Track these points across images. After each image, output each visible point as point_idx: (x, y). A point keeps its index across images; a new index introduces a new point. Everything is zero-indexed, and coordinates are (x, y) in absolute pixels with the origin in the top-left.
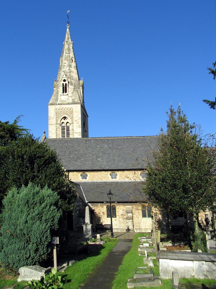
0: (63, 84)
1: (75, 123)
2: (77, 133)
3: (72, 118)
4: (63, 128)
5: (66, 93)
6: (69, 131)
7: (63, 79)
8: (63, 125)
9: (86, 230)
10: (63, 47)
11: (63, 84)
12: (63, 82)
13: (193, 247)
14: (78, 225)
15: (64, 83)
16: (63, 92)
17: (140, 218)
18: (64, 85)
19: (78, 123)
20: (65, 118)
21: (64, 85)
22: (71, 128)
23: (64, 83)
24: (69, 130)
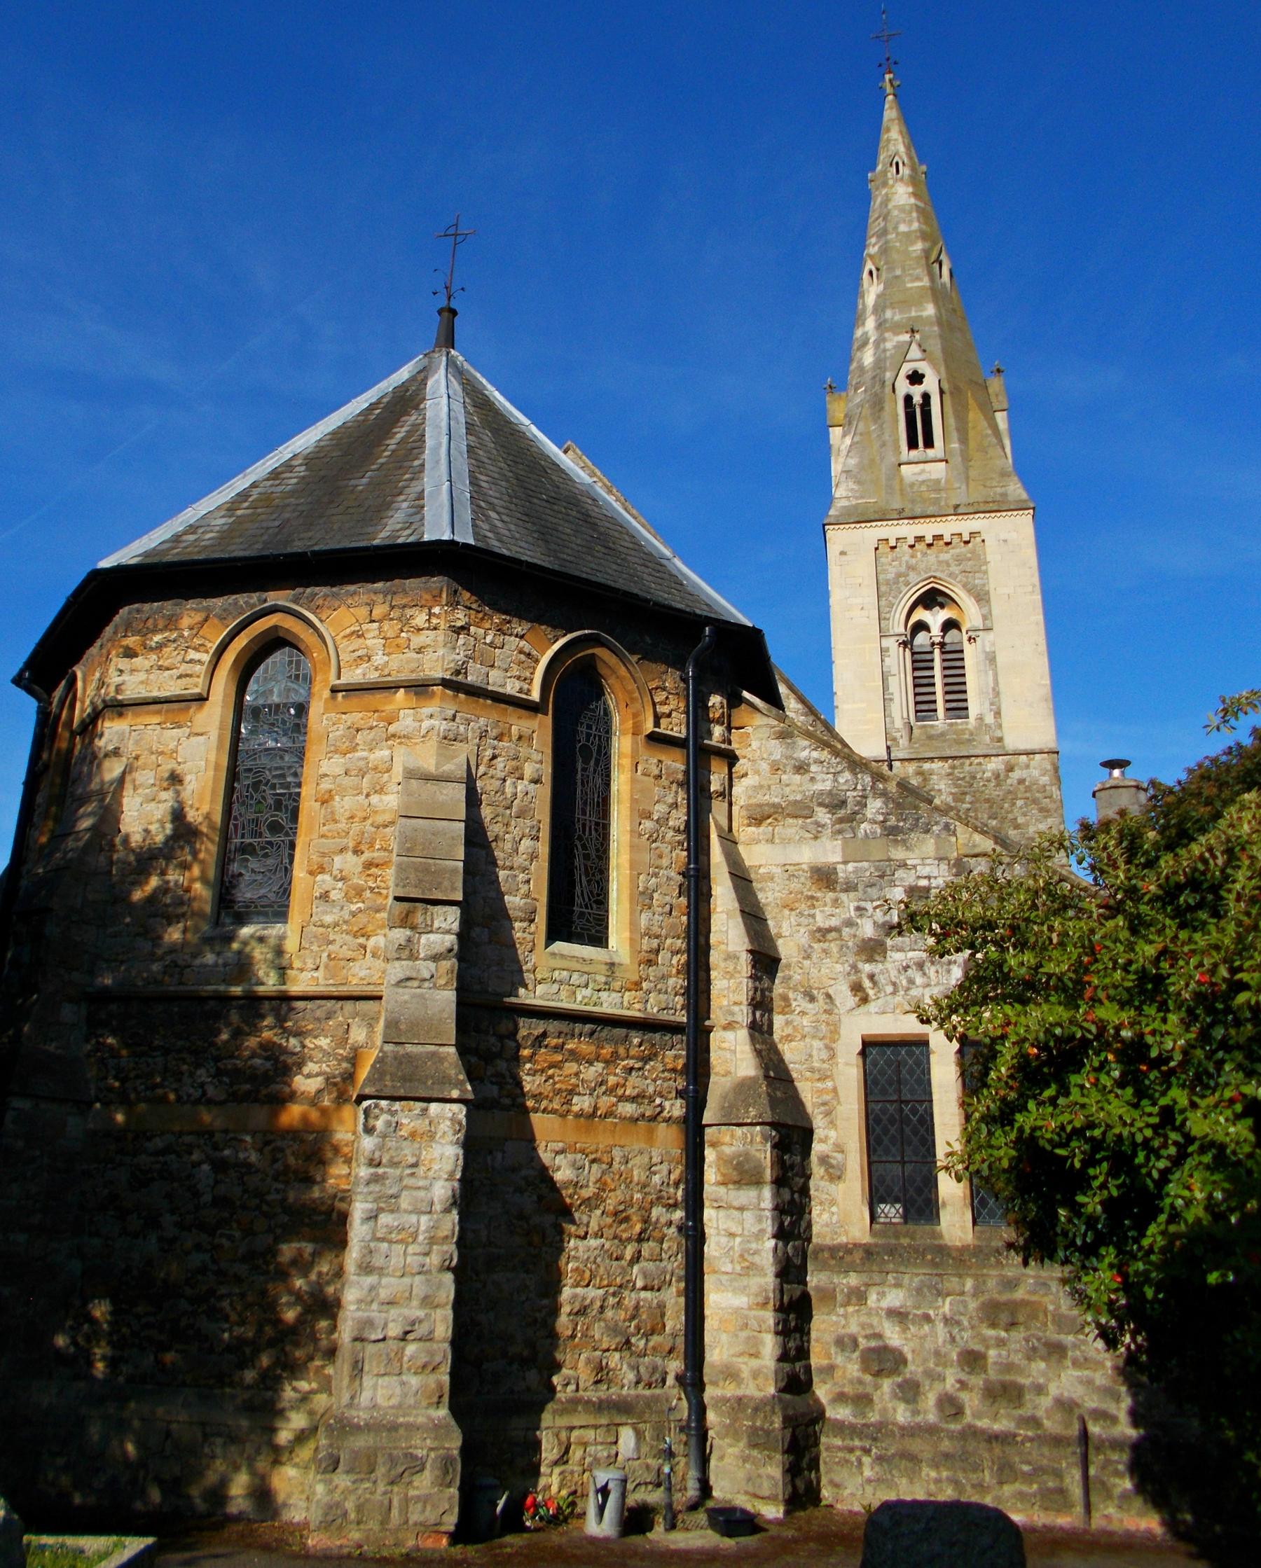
0: (908, 399)
3: (982, 597)
4: (921, 663)
5: (928, 451)
6: (958, 664)
7: (907, 368)
8: (921, 639)
9: (257, 1481)
10: (904, 130)
11: (908, 399)
12: (903, 387)
13: (1013, 1153)
14: (1218, 1528)
16: (912, 444)
17: (358, 1035)
18: (917, 399)
20: (932, 599)
21: (917, 399)
22: (971, 655)
23: (917, 392)
24: (958, 664)
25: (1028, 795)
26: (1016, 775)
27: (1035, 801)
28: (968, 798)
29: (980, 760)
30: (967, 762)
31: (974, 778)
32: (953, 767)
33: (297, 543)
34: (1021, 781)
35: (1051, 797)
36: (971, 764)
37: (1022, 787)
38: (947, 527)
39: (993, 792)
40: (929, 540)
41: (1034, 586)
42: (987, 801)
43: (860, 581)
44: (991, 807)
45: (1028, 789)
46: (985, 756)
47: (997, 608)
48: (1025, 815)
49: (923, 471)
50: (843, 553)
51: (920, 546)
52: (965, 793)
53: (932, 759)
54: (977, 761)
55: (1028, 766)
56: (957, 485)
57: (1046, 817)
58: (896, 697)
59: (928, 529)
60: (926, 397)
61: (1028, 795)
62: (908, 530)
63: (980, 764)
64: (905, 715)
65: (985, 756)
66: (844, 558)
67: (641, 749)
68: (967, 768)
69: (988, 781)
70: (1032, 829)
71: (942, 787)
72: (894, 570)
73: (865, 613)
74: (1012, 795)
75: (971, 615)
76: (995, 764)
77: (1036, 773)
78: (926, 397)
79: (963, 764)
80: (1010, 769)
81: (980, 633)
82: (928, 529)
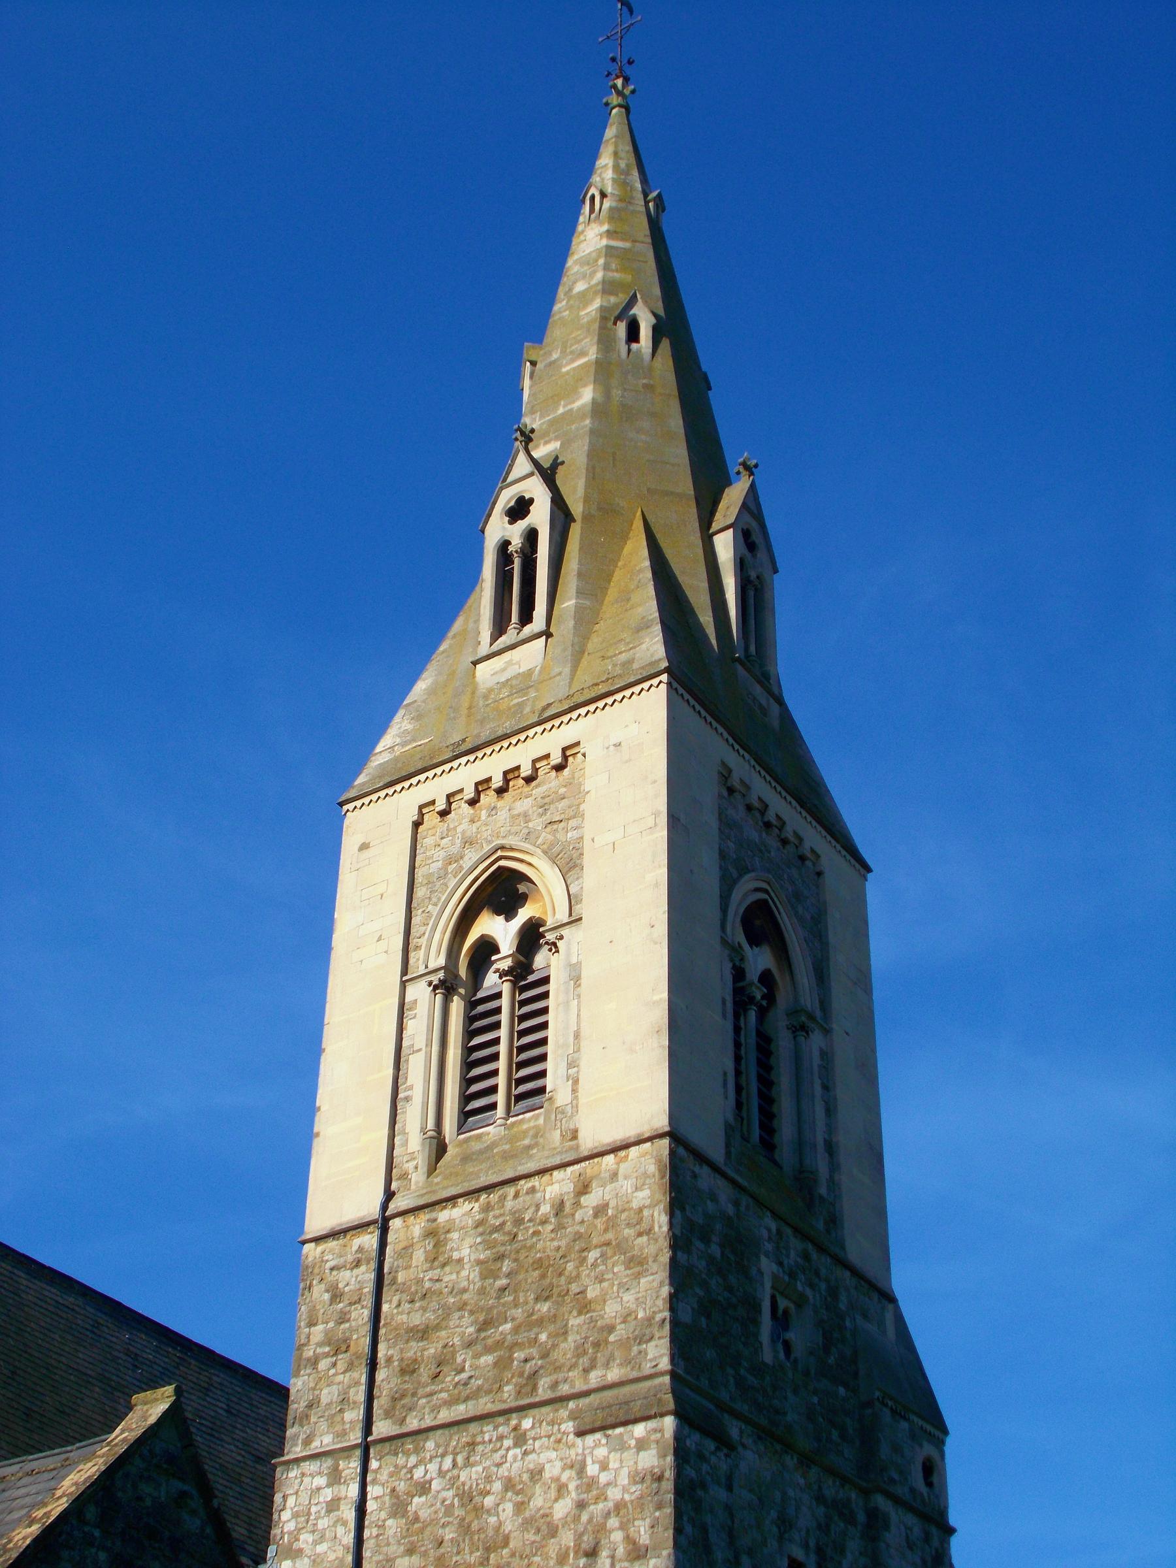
4: (479, 1019)
21: (516, 542)
25: (610, 1236)
26: (590, 1200)
27: (620, 1247)
28: (506, 1266)
29: (535, 1182)
30: (511, 1190)
31: (519, 1222)
32: (487, 1208)
33: (407, 725)
34: (600, 1210)
35: (649, 1231)
36: (516, 1196)
37: (600, 1223)
38: (520, 755)
39: (548, 1244)
40: (497, 782)
41: (656, 814)
42: (539, 1264)
43: (381, 889)
44: (543, 1276)
45: (612, 1223)
46: (542, 1172)
47: (589, 880)
48: (600, 1279)
49: (510, 663)
50: (364, 847)
51: (488, 798)
52: (500, 1257)
53: (452, 1200)
54: (524, 1185)
55: (614, 1176)
56: (557, 670)
57: (638, 1276)
58: (417, 1094)
59: (492, 765)
60: (531, 536)
61: (610, 1236)
62: (464, 775)
63: (533, 1190)
64: (431, 1124)
65: (542, 1172)
66: (366, 854)
67: (286, 1458)
68: (509, 1204)
69: (544, 1222)
70: (611, 1310)
71: (465, 1252)
72: (442, 854)
73: (383, 945)
74: (582, 1242)
75: (548, 899)
76: (559, 1185)
77: (625, 1185)
78: (531, 536)
79: (503, 1198)
80: (583, 1188)
81: (565, 932)
82: (492, 765)
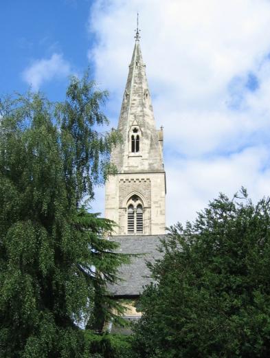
1: (153, 206)
2: (157, 224)
3: (149, 198)
11: (133, 137)
15: (135, 135)
16: (133, 151)
18: (135, 137)
19: (160, 207)
21: (135, 137)
